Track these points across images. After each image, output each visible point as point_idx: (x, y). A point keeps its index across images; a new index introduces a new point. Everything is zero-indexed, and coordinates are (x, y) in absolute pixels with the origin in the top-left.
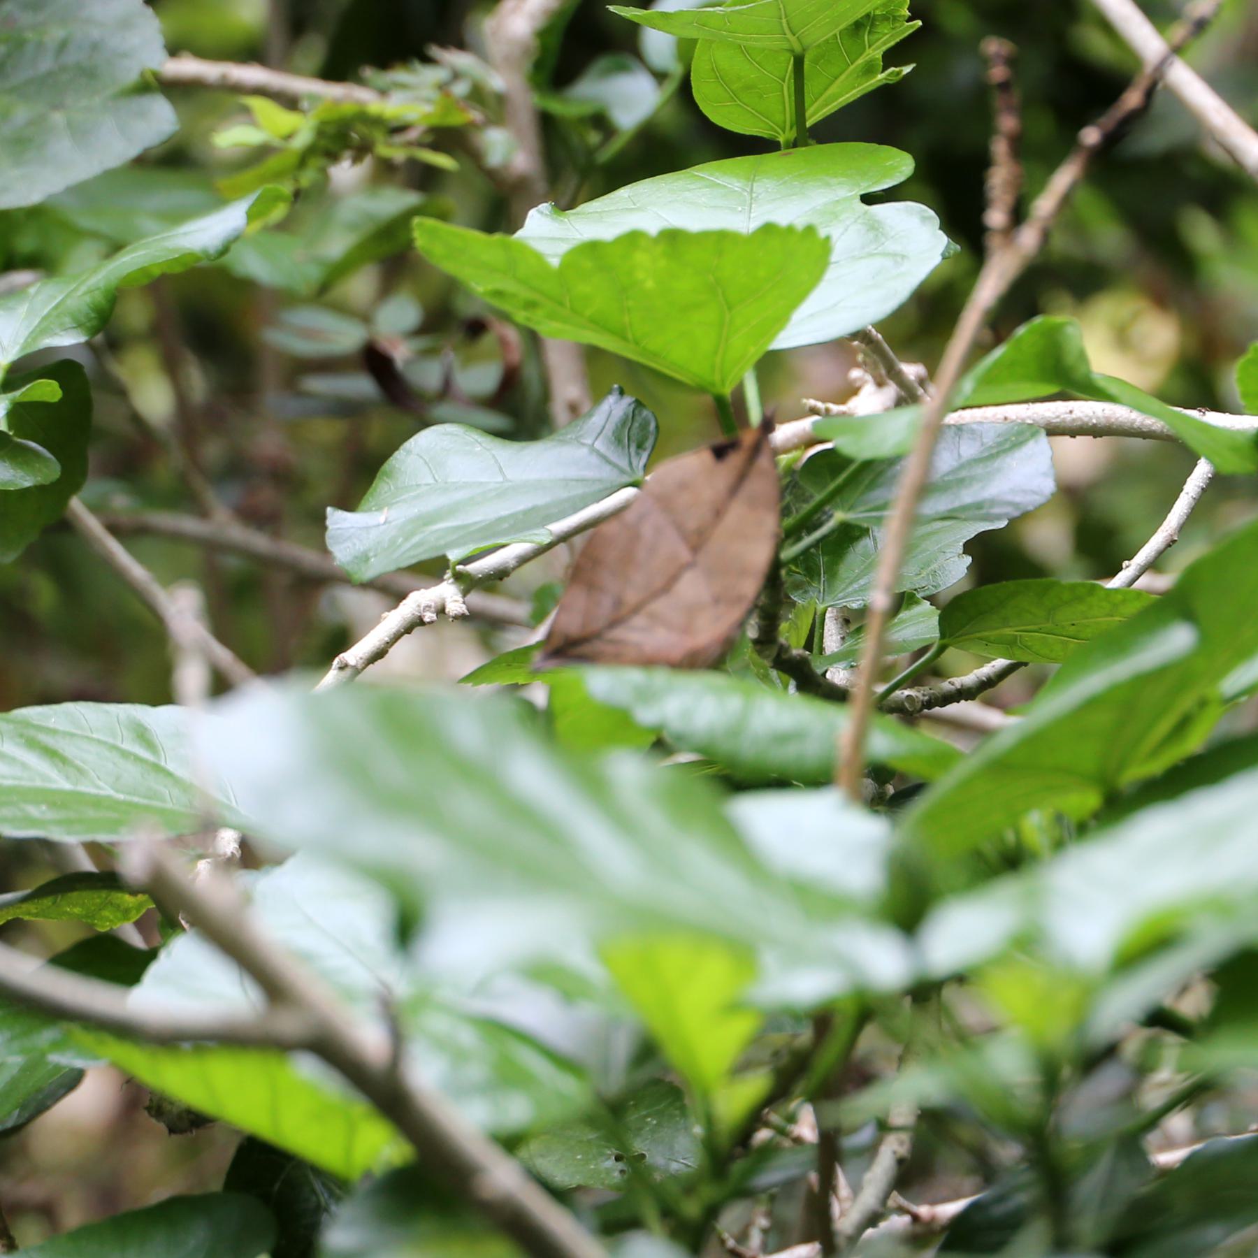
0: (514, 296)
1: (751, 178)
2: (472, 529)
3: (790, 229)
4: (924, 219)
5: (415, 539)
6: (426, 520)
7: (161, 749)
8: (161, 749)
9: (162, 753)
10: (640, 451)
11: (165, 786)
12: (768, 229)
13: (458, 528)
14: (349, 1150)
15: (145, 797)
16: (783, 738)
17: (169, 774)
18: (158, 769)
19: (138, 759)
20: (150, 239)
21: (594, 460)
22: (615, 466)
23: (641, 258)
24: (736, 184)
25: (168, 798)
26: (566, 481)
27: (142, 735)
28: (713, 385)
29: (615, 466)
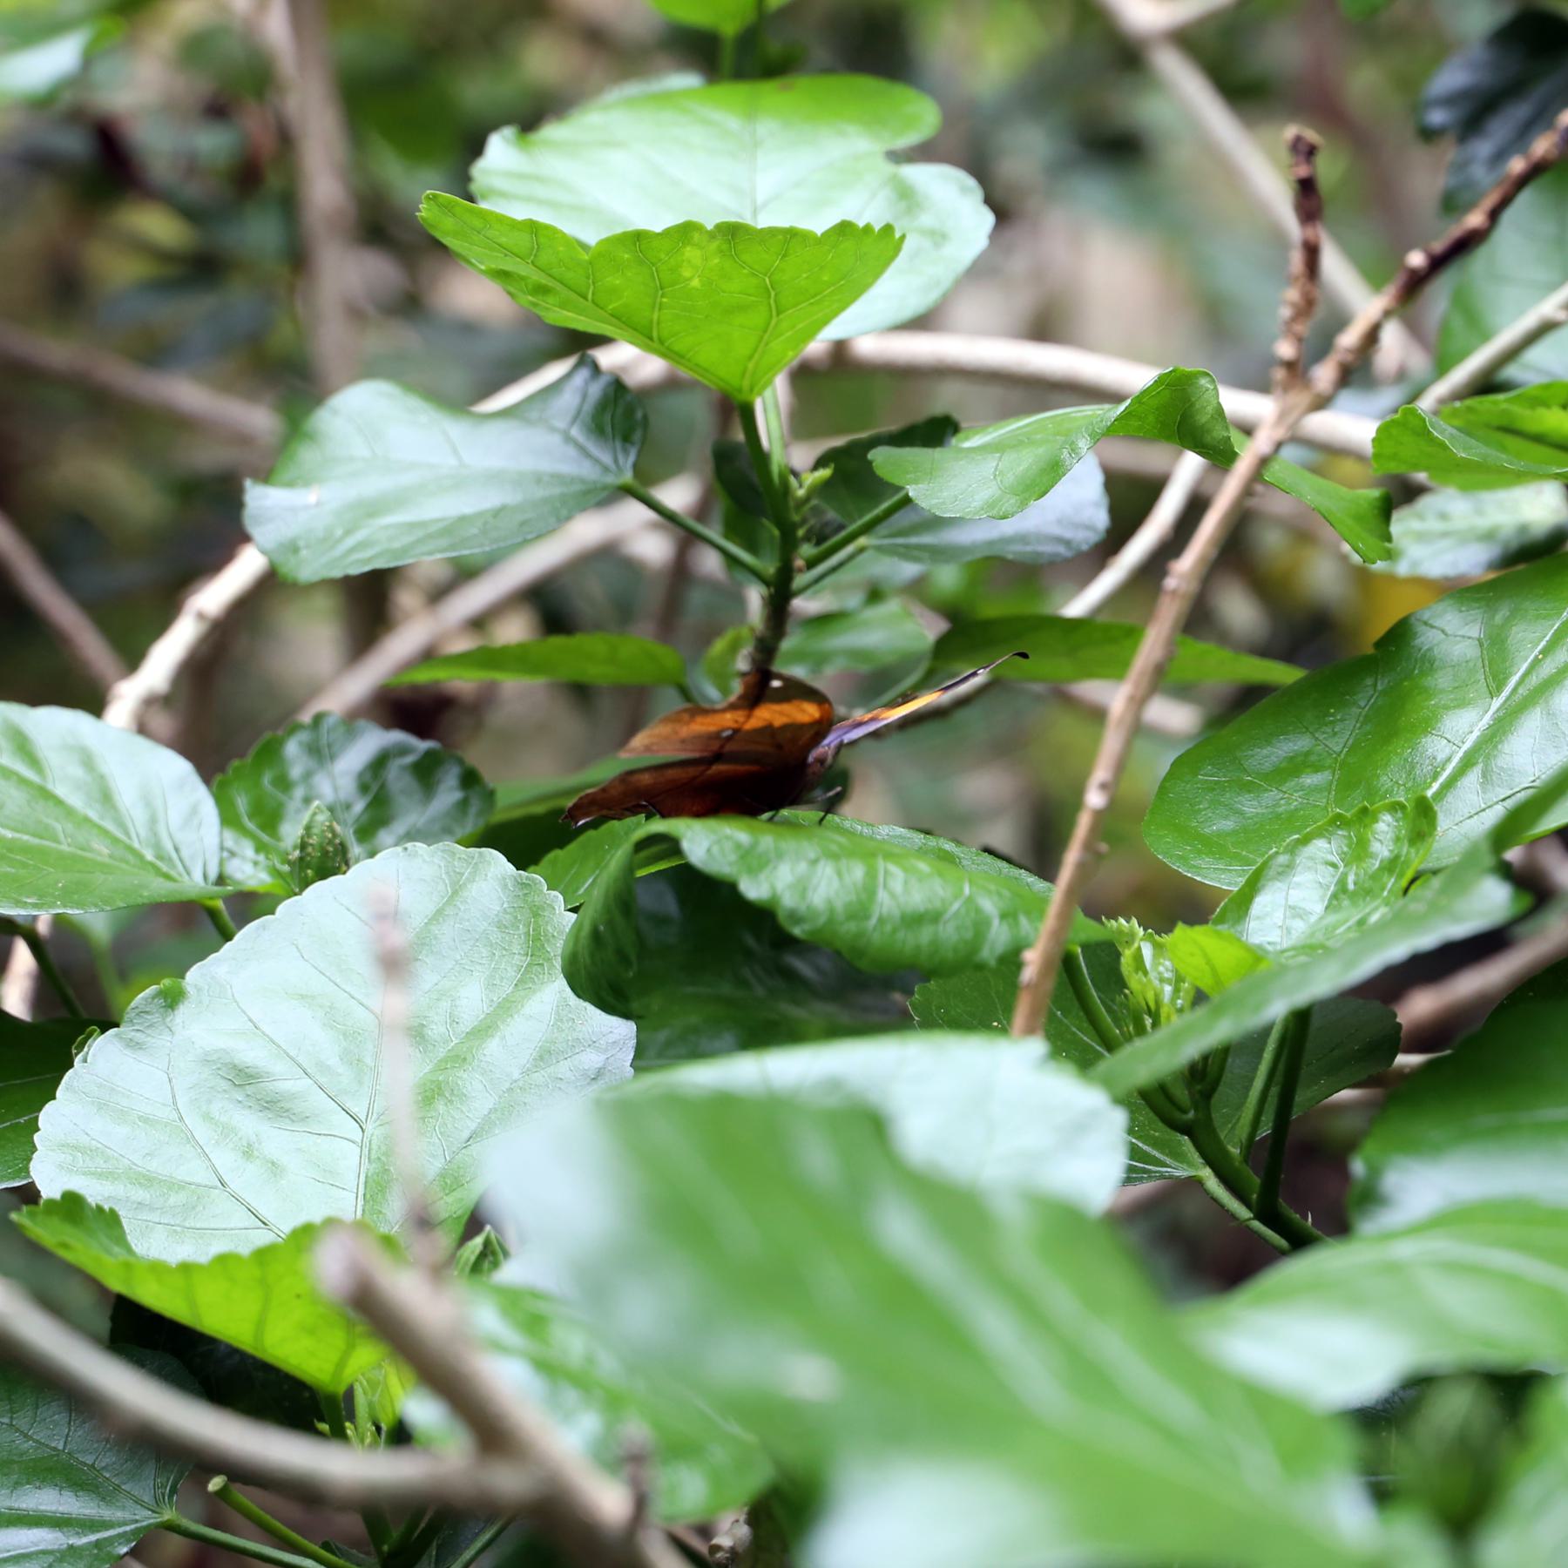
0: (522, 278)
1: (751, 115)
2: (432, 529)
3: (868, 229)
4: (964, 190)
5: (359, 536)
6: (371, 508)
7: (51, 777)
8: (51, 777)
9: (49, 773)
10: (628, 445)
11: (57, 820)
12: (844, 228)
13: (412, 526)
14: (341, 1365)
15: (34, 835)
16: (915, 920)
17: (59, 802)
18: (45, 795)
19: (22, 781)
20: (439, 556)
21: (571, 451)
22: (597, 461)
23: (690, 253)
24: (733, 122)
25: (61, 836)
26: (538, 479)
27: (23, 745)
28: (740, 390)
29: (597, 461)
